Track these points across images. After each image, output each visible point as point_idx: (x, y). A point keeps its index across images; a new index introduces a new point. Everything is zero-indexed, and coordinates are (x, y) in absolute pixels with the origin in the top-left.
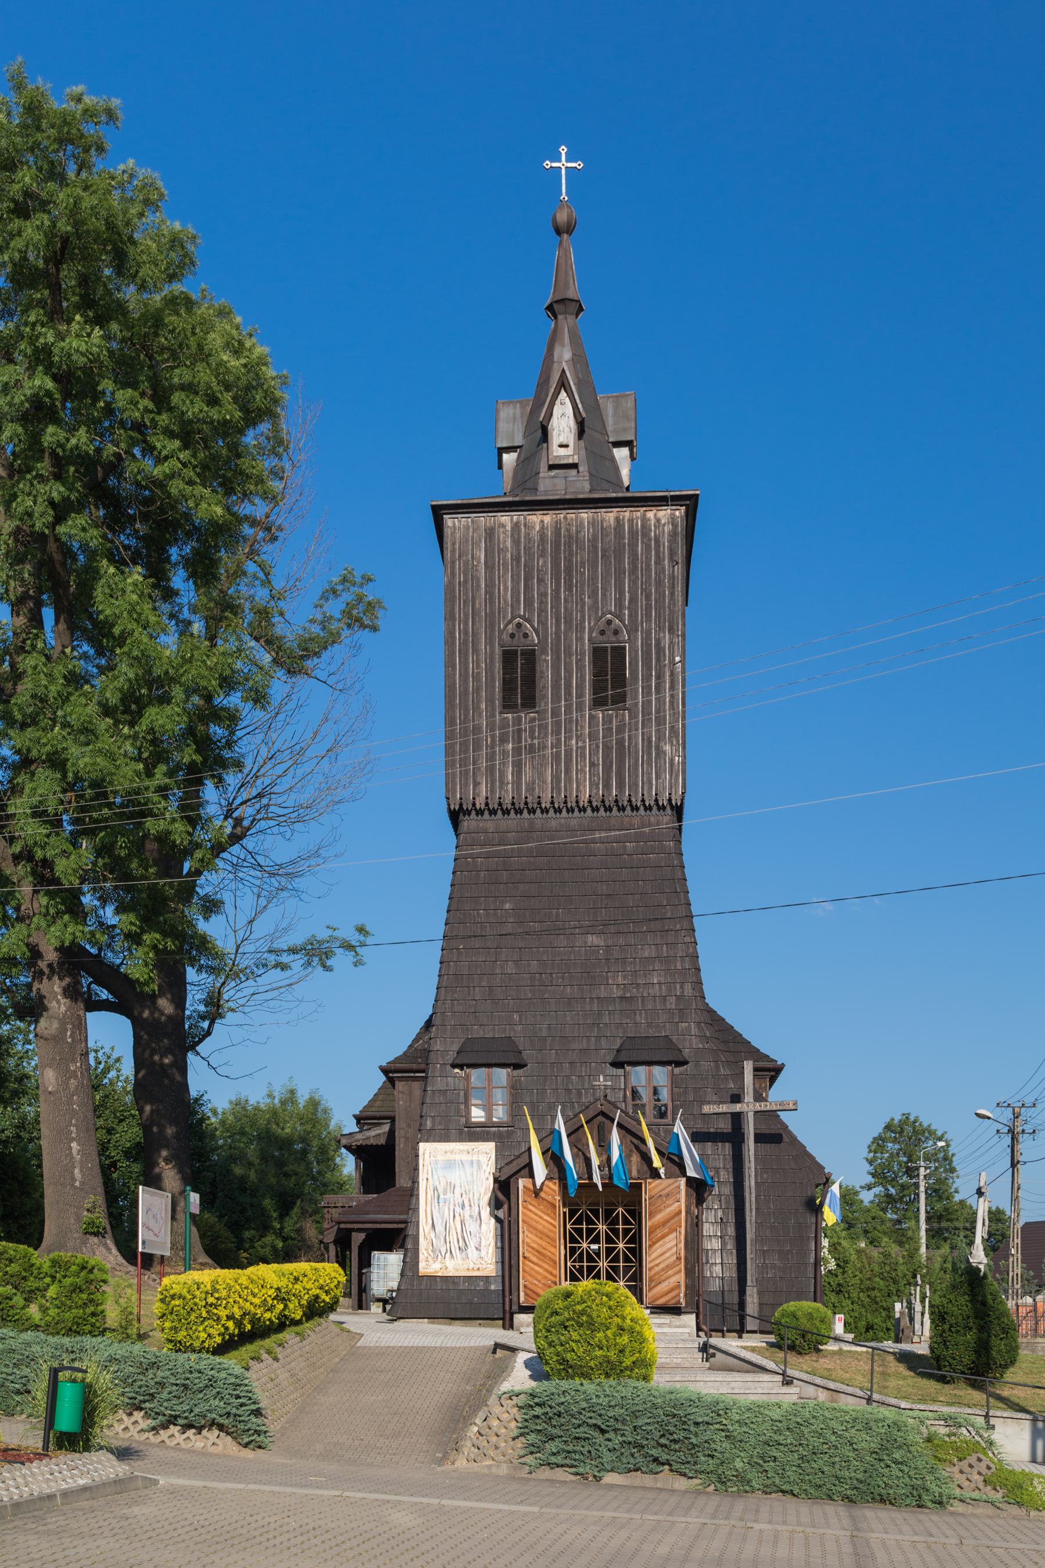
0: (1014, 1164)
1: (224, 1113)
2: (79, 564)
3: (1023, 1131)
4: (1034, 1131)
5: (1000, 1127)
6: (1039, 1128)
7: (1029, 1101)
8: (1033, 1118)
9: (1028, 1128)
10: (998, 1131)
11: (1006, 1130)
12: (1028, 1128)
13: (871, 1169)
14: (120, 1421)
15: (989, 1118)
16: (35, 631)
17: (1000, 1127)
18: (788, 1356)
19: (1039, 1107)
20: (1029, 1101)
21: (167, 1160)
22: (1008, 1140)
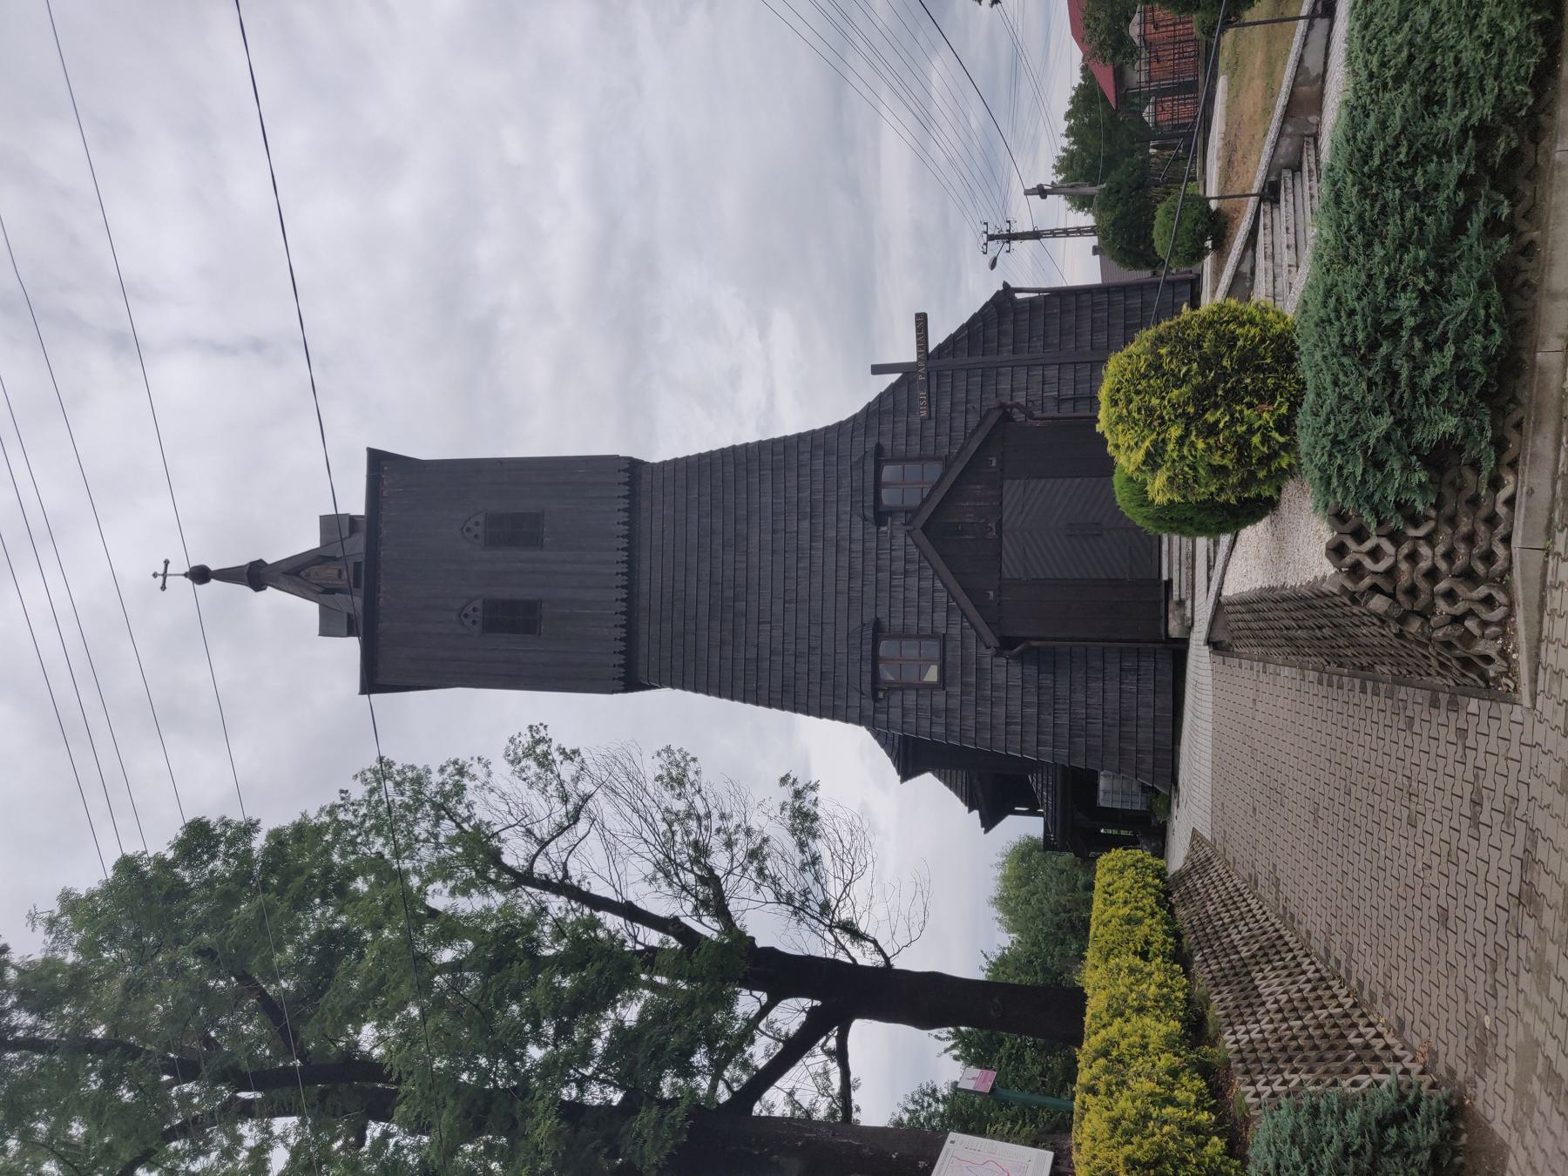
3: (1009, 231)
4: (1009, 222)
10: (1008, 252)
11: (1007, 245)
22: (1015, 244)
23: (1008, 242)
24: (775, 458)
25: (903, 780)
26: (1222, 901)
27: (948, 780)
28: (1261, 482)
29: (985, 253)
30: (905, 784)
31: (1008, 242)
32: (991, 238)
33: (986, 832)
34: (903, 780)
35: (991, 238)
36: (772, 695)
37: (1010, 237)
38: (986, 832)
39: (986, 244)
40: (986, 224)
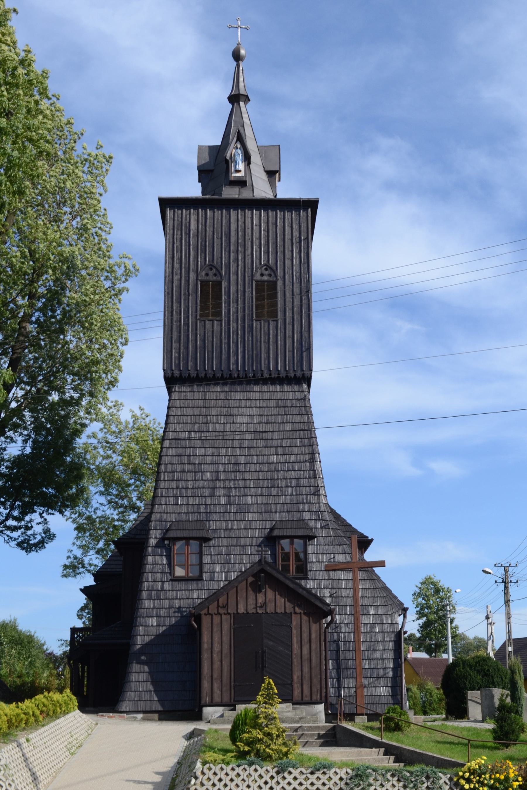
0: (507, 602)
1: (10, 715)
2: (66, 265)
3: (511, 582)
4: (517, 582)
5: (497, 579)
6: (520, 579)
7: (513, 563)
8: (515, 574)
9: (514, 580)
10: (496, 582)
11: (501, 580)
12: (514, 580)
13: (75, 526)
14: (318, 778)
15: (490, 573)
16: (59, 283)
17: (497, 579)
18: (390, 652)
19: (519, 566)
20: (513, 563)
21: (200, 762)
22: (502, 586)
23: (503, 582)
24: (238, 449)
25: (71, 628)
26: (41, 763)
27: (125, 537)
28: (47, 324)
29: (495, 565)
30: (80, 591)
31: (503, 582)
32: (506, 571)
33: (81, 590)
34: (71, 628)
35: (506, 571)
36: (189, 417)
37: (505, 582)
38: (81, 590)
39: (502, 566)
40: (516, 566)
